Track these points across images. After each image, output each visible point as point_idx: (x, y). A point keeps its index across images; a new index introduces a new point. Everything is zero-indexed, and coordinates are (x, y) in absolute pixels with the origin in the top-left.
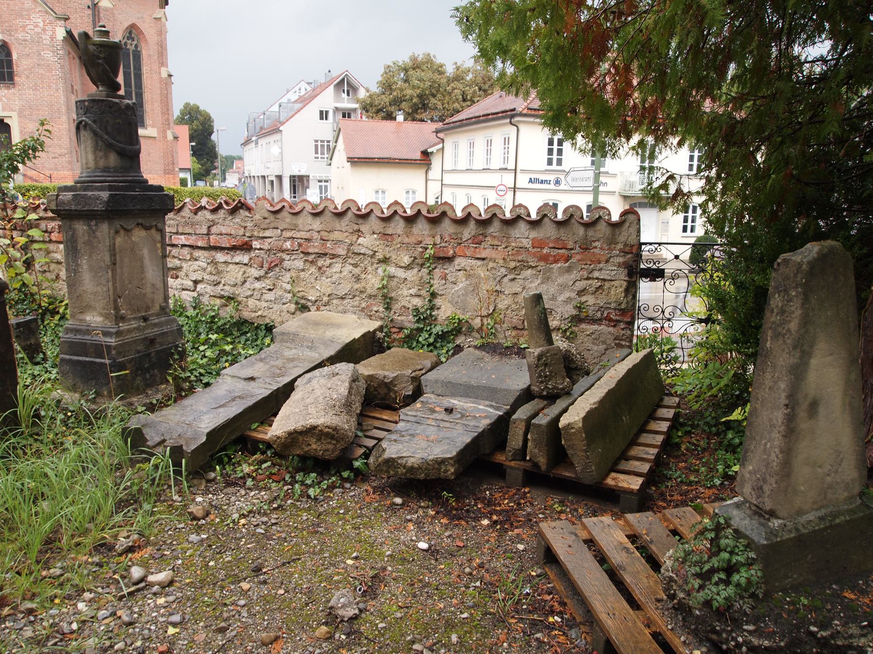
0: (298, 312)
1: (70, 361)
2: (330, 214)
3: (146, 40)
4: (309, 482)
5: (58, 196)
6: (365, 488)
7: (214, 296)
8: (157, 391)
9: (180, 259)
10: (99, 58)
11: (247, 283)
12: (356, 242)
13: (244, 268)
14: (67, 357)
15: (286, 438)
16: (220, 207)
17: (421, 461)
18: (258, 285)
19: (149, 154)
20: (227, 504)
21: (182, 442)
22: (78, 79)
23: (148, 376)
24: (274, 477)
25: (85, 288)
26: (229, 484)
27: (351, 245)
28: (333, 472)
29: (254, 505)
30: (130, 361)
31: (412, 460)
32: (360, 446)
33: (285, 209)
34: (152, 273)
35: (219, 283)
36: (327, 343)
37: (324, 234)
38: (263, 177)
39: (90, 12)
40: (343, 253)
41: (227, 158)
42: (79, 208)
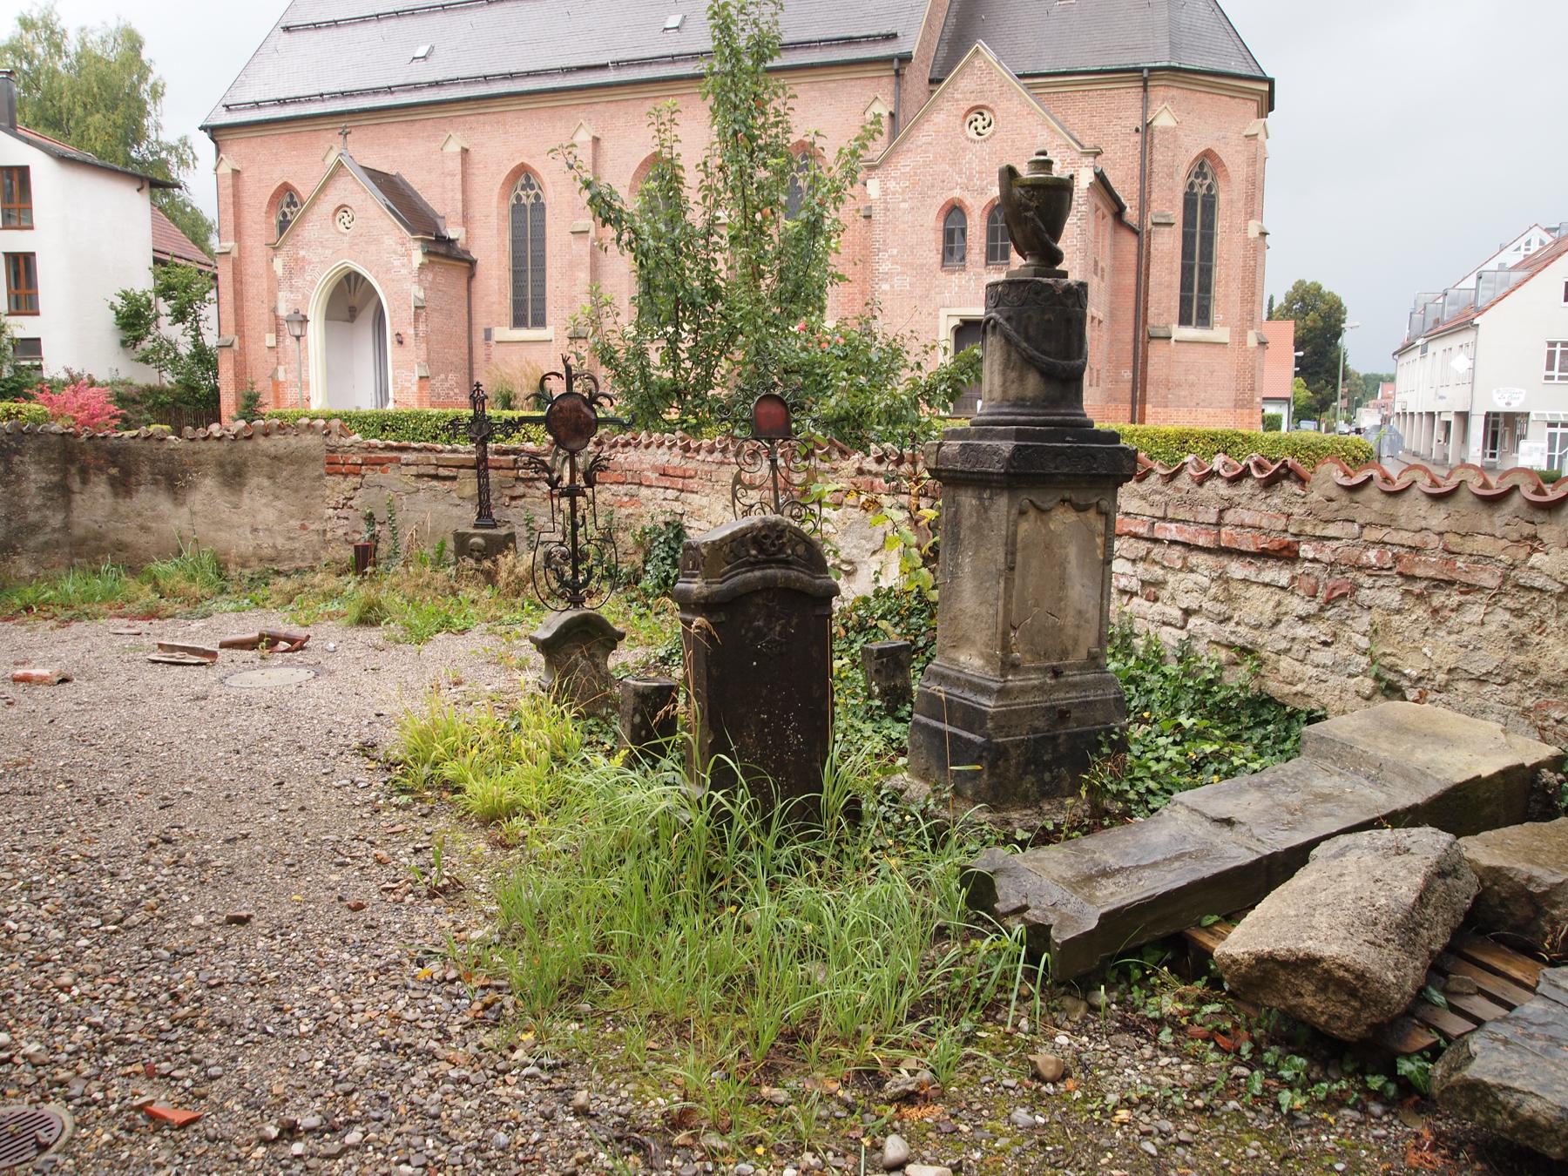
0: (1378, 697)
1: (926, 726)
2: (1471, 498)
3: (1227, 175)
4: (1287, 1074)
5: (940, 445)
6: (1417, 1128)
7: (1218, 643)
8: (1062, 807)
9: (1164, 567)
10: (1027, 208)
11: (1282, 626)
12: (1525, 562)
13: (1280, 595)
14: (923, 719)
15: (1250, 966)
16: (1246, 473)
17: (1558, 1113)
18: (1302, 631)
19: (1212, 372)
20: (1109, 1068)
21: (1053, 919)
22: (1107, 249)
23: (1047, 776)
24: (1221, 1039)
25: (963, 606)
26: (1126, 1027)
27: (1513, 567)
28: (1349, 1068)
29: (1159, 1086)
30: (1017, 745)
31: (1535, 1104)
32: (1429, 1026)
33: (1373, 484)
34: (1079, 591)
35: (1229, 619)
36: (1410, 777)
37: (1452, 539)
38: (1431, 415)
39: (1138, 138)
40: (1493, 582)
41: (1366, 378)
42: (967, 467)
